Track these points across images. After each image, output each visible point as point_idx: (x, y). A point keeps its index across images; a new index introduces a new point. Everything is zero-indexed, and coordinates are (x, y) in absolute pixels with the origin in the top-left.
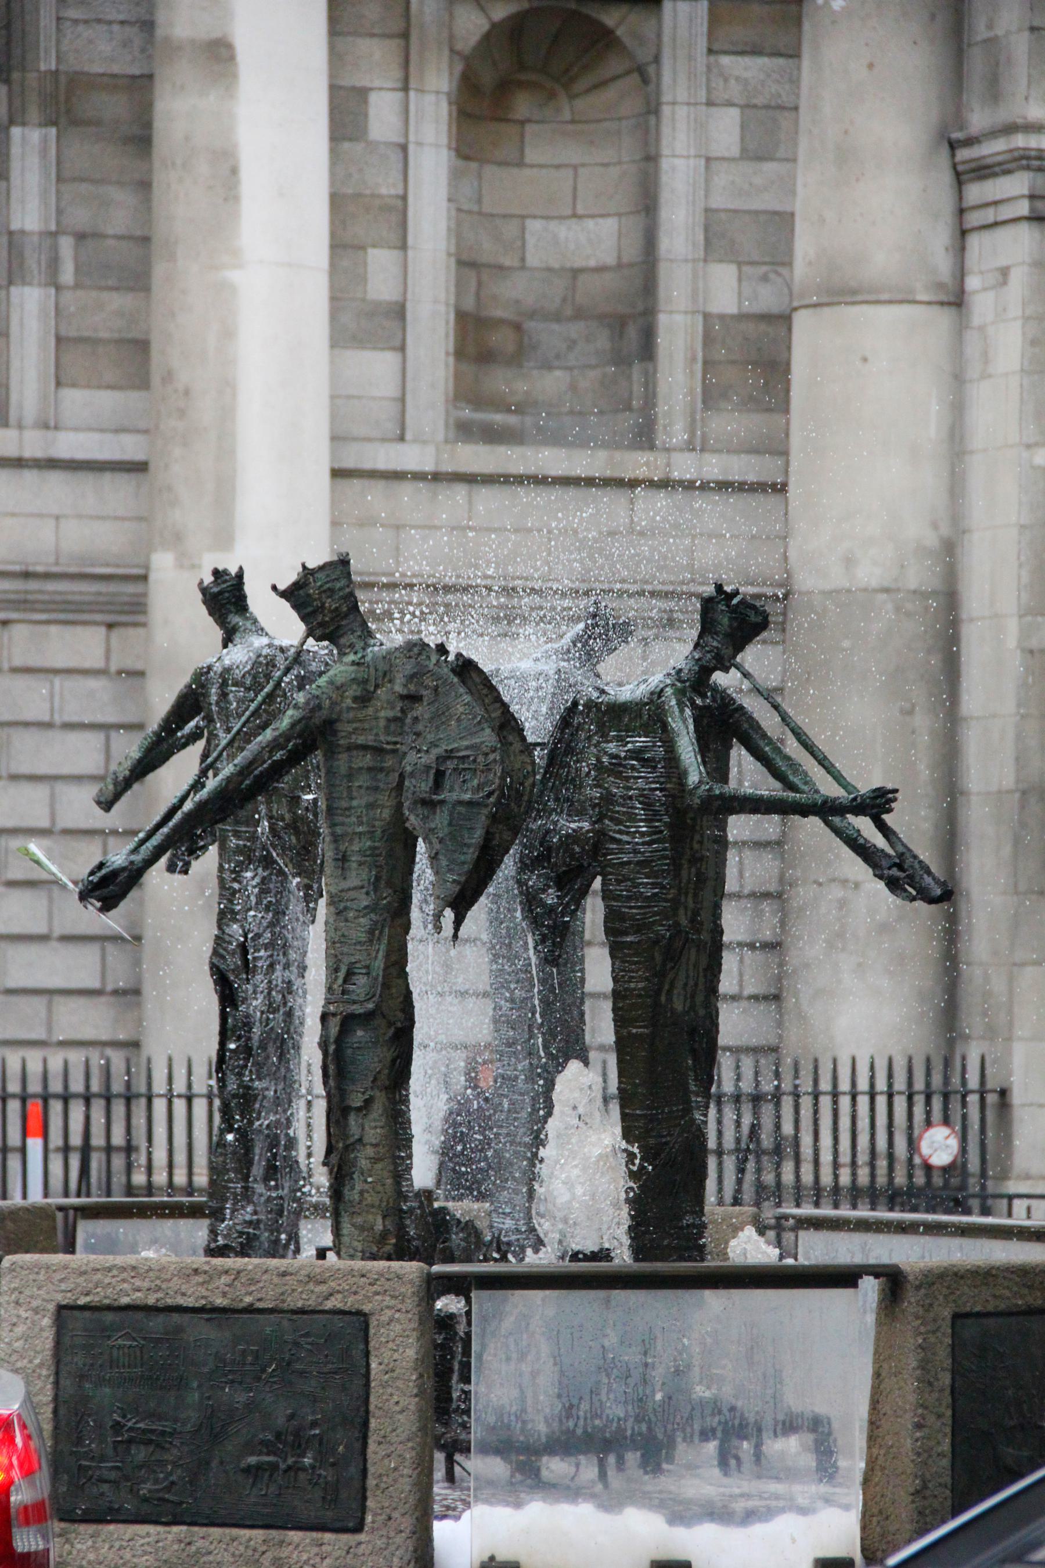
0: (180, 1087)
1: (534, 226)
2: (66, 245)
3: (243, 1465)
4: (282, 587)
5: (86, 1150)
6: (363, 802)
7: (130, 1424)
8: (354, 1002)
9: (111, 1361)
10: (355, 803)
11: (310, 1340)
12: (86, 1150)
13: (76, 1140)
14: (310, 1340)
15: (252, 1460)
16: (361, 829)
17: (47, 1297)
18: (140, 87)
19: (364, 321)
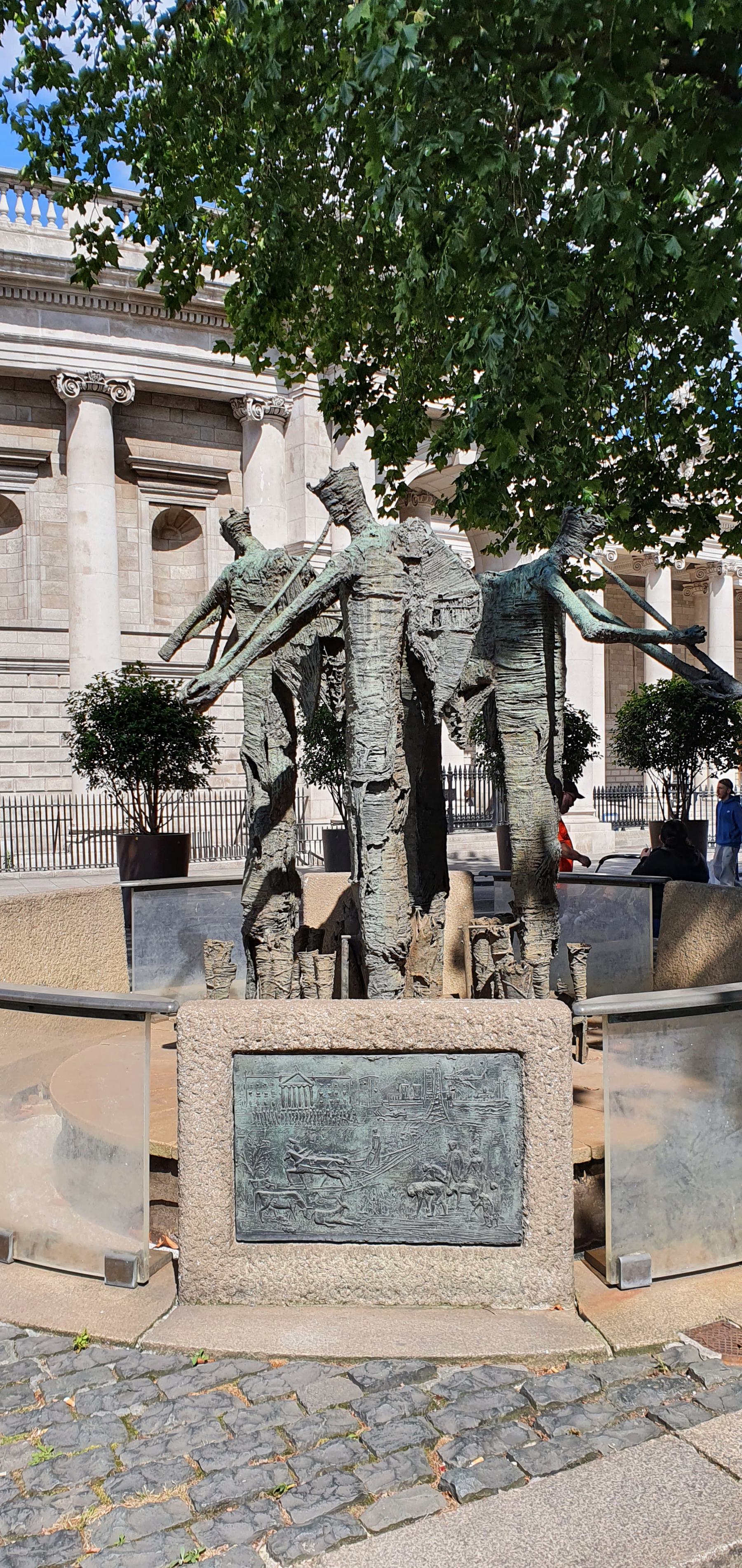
0: (85, 803)
1: (173, 568)
2: (43, 568)
3: (412, 1191)
4: (313, 485)
5: (58, 820)
6: (378, 635)
7: (303, 1157)
8: (376, 773)
9: (283, 1101)
10: (372, 636)
11: (468, 1077)
12: (58, 820)
13: (55, 818)
14: (468, 1077)
15: (420, 1186)
16: (376, 654)
17: (221, 1043)
18: (63, 526)
19: (125, 591)
